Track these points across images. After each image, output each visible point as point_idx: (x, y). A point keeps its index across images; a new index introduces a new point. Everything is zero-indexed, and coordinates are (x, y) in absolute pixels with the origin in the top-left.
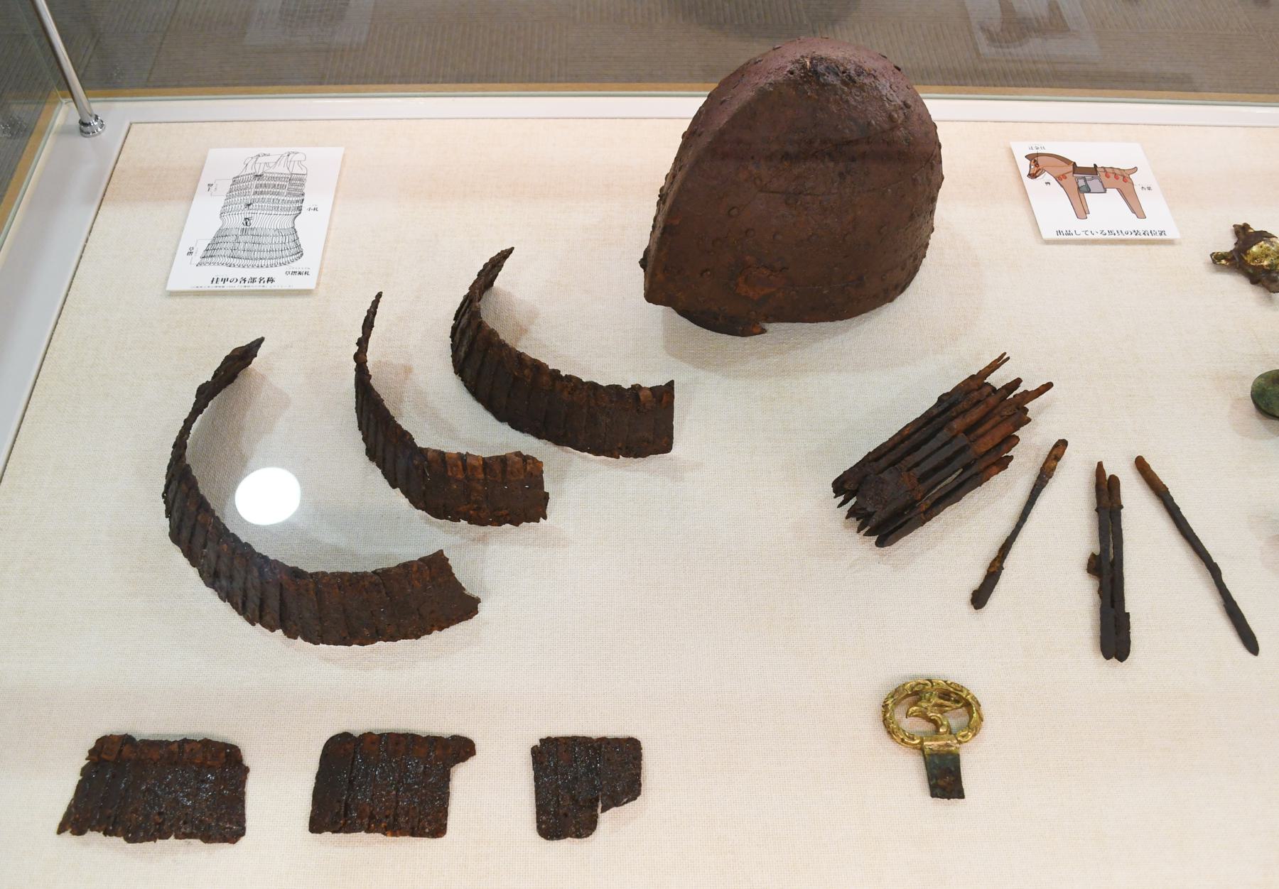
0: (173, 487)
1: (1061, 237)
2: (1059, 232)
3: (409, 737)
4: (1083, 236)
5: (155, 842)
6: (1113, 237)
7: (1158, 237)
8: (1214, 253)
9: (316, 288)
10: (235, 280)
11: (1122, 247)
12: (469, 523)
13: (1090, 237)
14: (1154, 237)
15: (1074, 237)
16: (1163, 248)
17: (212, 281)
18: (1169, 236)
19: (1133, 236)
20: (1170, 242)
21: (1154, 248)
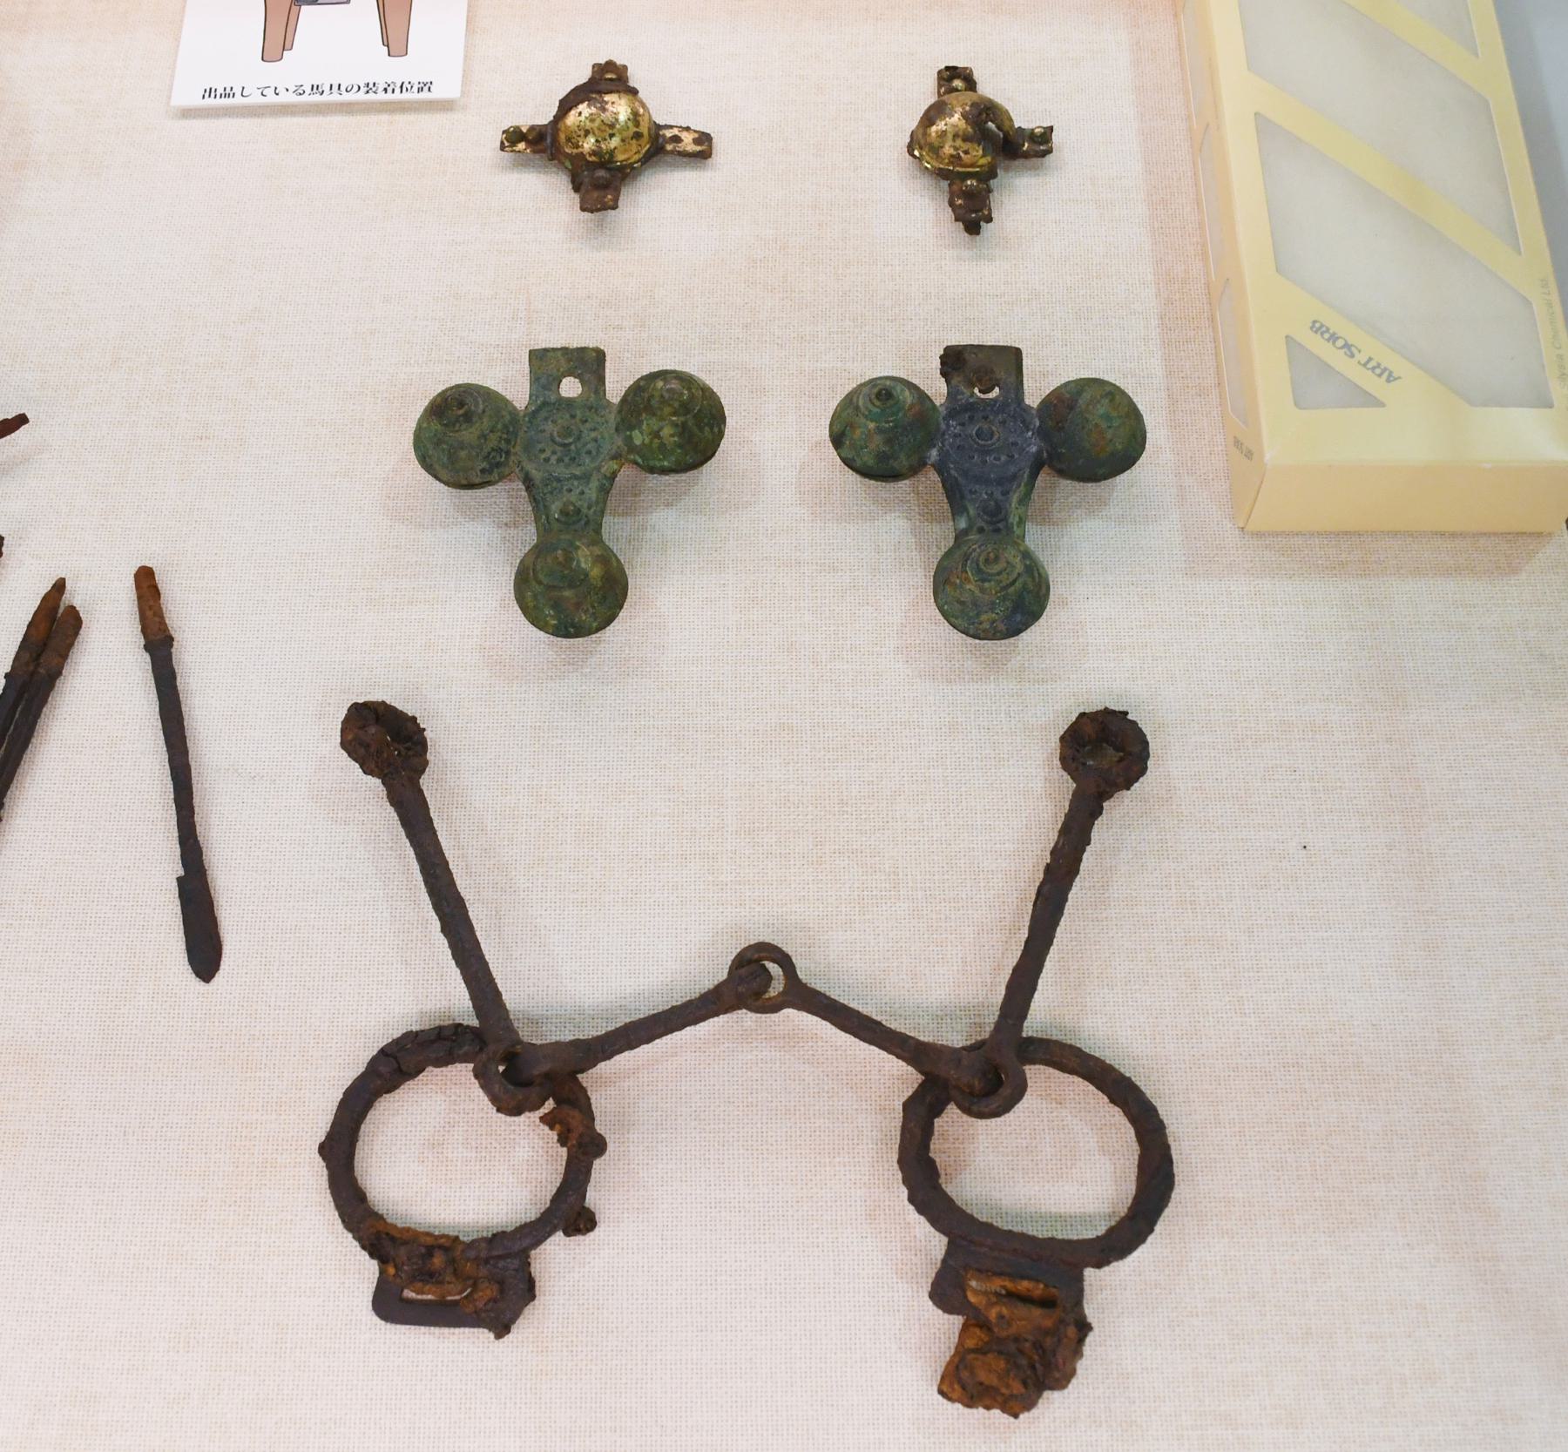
0: (709, 454)
1: (210, 101)
2: (210, 92)
3: (951, 1263)
4: (255, 99)
5: (424, 730)
6: (317, 98)
7: (413, 96)
8: (502, 143)
9: (463, 93)
10: (356, 88)
11: (336, 120)
12: (1089, 844)
13: (271, 98)
14: (406, 96)
15: (238, 100)
16: (440, 118)
17: (204, 97)
18: (437, 93)
19: (361, 96)
20: (445, 106)
21: (401, 119)
